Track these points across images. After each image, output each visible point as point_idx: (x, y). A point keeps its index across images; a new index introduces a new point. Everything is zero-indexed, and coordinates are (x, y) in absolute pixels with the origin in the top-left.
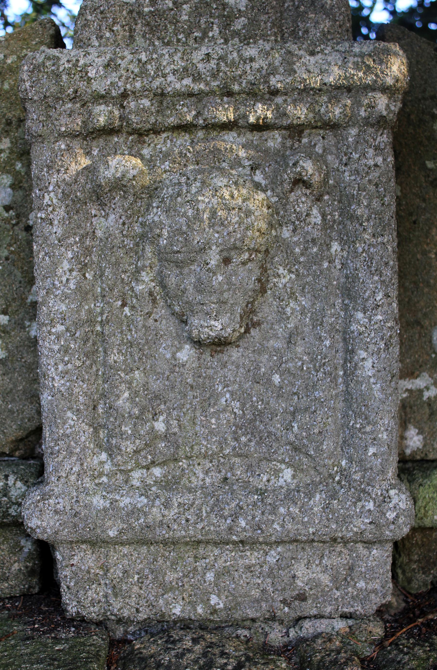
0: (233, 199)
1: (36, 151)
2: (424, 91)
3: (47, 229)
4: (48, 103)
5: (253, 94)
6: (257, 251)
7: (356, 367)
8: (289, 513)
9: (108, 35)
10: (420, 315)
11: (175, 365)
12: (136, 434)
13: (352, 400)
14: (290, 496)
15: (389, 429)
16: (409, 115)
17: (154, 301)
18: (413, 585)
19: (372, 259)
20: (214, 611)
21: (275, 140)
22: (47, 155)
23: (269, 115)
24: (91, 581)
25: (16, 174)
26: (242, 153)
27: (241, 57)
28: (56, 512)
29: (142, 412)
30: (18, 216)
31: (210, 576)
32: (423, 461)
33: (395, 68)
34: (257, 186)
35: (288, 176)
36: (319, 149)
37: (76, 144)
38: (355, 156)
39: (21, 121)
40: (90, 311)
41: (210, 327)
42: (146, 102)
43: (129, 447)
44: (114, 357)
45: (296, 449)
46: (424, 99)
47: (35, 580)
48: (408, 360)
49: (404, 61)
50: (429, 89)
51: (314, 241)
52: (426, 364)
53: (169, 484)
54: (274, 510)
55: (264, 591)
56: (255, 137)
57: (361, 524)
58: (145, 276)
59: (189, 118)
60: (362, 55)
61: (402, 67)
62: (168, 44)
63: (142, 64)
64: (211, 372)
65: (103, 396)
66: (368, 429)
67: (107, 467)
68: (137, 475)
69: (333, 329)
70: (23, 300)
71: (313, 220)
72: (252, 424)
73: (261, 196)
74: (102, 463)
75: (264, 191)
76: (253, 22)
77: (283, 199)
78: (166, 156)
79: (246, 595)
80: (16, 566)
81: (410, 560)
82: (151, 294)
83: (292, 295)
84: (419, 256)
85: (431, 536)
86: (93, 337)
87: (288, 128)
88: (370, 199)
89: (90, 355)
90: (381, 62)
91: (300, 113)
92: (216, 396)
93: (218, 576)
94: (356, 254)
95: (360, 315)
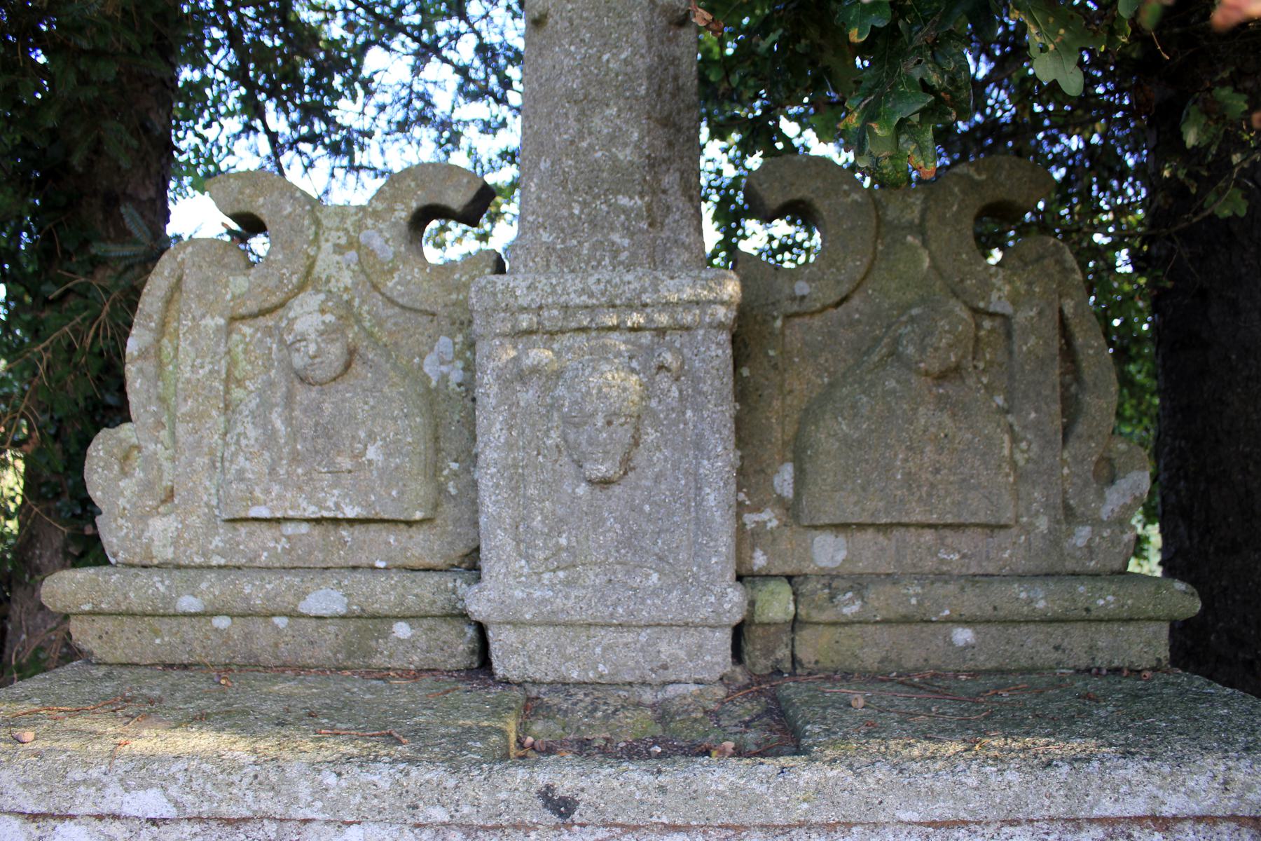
0: (617, 381)
1: (479, 345)
3: (485, 400)
4: (488, 313)
5: (630, 307)
6: (631, 416)
7: (703, 500)
8: (654, 604)
9: (531, 264)
11: (574, 498)
12: (546, 547)
13: (702, 524)
14: (655, 592)
17: (560, 451)
19: (714, 422)
20: (601, 676)
21: (646, 338)
22: (486, 350)
23: (642, 321)
24: (513, 652)
25: (466, 360)
26: (623, 347)
27: (621, 280)
28: (489, 600)
29: (550, 531)
30: (467, 391)
31: (598, 650)
32: (767, 576)
33: (730, 288)
34: (633, 371)
35: (654, 363)
36: (677, 345)
37: (507, 342)
38: (702, 349)
39: (470, 322)
40: (514, 459)
41: (598, 470)
42: (555, 312)
43: (541, 555)
44: (531, 491)
45: (660, 559)
47: (475, 658)
51: (673, 409)
53: (569, 583)
54: (643, 601)
55: (637, 662)
56: (632, 336)
57: (705, 612)
58: (553, 434)
59: (585, 323)
60: (707, 280)
62: (573, 271)
63: (553, 286)
64: (600, 503)
65: (523, 519)
66: (712, 544)
67: (525, 570)
68: (546, 576)
69: (687, 472)
70: (469, 452)
71: (672, 394)
72: (629, 541)
73: (634, 378)
74: (522, 567)
75: (638, 374)
76: (633, 255)
77: (652, 379)
78: (569, 349)
79: (625, 665)
80: (461, 647)
82: (557, 446)
83: (658, 448)
86: (516, 477)
87: (656, 329)
88: (713, 380)
89: (515, 489)
90: (720, 284)
91: (663, 319)
92: (604, 520)
93: (604, 650)
94: (703, 419)
95: (705, 462)
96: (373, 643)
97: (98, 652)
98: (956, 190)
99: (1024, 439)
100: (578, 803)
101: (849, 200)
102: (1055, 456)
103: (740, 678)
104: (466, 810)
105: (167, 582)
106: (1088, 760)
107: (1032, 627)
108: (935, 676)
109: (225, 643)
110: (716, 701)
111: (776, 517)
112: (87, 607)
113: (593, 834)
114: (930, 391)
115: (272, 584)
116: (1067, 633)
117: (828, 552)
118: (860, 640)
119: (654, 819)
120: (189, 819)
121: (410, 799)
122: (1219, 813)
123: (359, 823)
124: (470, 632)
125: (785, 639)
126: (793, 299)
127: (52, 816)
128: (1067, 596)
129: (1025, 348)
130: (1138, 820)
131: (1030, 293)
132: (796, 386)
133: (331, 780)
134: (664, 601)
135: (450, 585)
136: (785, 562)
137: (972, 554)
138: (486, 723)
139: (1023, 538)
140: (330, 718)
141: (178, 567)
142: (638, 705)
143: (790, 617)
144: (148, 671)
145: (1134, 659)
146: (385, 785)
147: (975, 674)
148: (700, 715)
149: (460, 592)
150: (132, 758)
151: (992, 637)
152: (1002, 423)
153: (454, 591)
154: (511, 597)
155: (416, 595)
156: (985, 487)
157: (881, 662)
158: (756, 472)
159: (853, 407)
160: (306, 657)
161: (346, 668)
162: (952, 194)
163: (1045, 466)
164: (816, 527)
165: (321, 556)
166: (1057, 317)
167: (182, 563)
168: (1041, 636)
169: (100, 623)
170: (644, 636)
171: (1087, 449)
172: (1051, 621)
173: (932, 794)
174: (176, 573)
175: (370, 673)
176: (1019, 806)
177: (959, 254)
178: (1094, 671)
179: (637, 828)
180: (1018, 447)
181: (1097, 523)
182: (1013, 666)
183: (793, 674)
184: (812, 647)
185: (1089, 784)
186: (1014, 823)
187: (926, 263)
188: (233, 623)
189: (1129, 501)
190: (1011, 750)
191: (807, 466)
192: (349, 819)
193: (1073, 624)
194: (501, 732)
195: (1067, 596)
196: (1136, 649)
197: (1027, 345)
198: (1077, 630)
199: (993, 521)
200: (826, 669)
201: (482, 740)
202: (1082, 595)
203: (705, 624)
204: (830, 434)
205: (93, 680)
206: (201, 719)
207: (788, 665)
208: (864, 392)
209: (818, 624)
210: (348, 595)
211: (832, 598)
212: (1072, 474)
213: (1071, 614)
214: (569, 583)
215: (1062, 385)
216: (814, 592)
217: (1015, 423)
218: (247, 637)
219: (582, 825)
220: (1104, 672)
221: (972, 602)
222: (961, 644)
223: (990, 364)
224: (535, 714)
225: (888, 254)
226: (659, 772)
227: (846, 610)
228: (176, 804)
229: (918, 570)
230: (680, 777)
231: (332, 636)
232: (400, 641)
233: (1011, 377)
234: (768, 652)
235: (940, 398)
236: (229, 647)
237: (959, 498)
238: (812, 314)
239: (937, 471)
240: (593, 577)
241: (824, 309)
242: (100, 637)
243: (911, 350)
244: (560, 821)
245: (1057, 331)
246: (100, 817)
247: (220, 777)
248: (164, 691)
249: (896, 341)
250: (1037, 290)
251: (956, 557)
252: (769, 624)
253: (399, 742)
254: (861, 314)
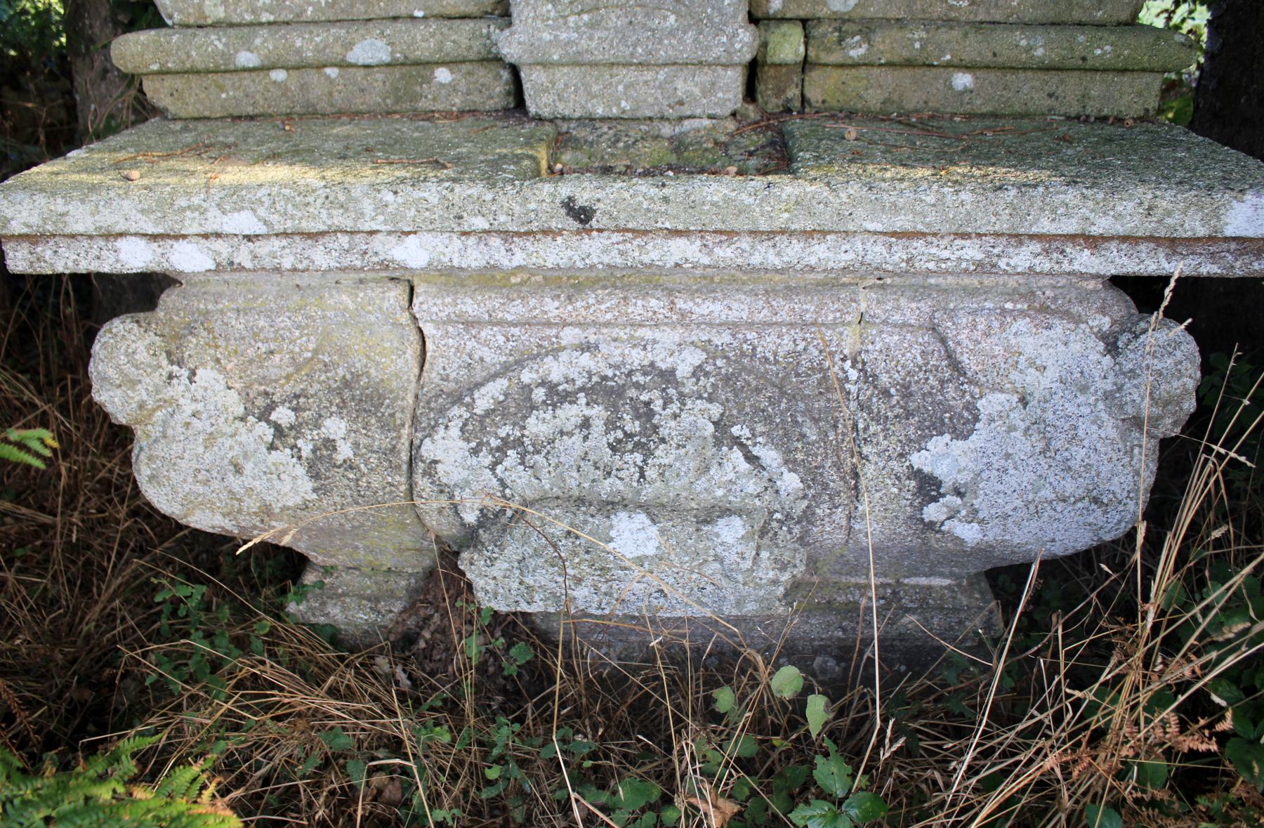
14: (672, 33)
20: (624, 112)
31: (621, 88)
47: (511, 99)
53: (593, 25)
54: (661, 41)
55: (656, 98)
57: (718, 52)
68: (572, 19)
74: (549, 11)
79: (645, 101)
80: (498, 89)
93: (626, 87)
96: (418, 88)
97: (172, 108)
100: (595, 211)
103: (752, 115)
104: (502, 218)
105: (224, 40)
106: (1035, 186)
107: (1030, 74)
108: (932, 117)
109: (284, 94)
110: (728, 134)
112: (155, 67)
113: (609, 238)
115: (320, 37)
116: (1062, 81)
118: (865, 82)
119: (659, 225)
120: (277, 235)
121: (456, 210)
122: (1139, 234)
123: (415, 233)
124: (506, 75)
127: (168, 236)
130: (1072, 238)
133: (389, 197)
134: (680, 41)
135: (485, 31)
138: (519, 151)
140: (384, 151)
141: (231, 25)
142: (657, 137)
143: (801, 58)
144: (219, 123)
145: (1123, 109)
146: (434, 199)
147: (970, 116)
148: (710, 145)
149: (494, 37)
150: (223, 187)
151: (991, 82)
153: (488, 36)
154: (540, 39)
155: (454, 42)
160: (359, 103)
161: (395, 112)
165: (362, 8)
167: (234, 21)
168: (1037, 84)
169: (169, 82)
170: (662, 75)
172: (1048, 69)
173: (895, 209)
174: (231, 31)
175: (417, 115)
176: (969, 222)
179: (645, 232)
183: (801, 112)
184: (820, 87)
185: (1032, 205)
186: (965, 236)
188: (289, 75)
190: (972, 176)
192: (406, 229)
194: (533, 158)
196: (1127, 98)
198: (1072, 79)
200: (832, 109)
201: (514, 163)
203: (717, 63)
205: (173, 132)
206: (274, 157)
207: (797, 104)
209: (826, 65)
210: (391, 44)
211: (840, 41)
213: (1068, 63)
214: (593, 25)
216: (824, 35)
218: (303, 87)
219: (600, 231)
220: (1092, 119)
221: (974, 47)
222: (960, 88)
224: (565, 146)
226: (664, 185)
227: (853, 53)
228: (265, 222)
229: (927, 16)
230: (681, 190)
231: (380, 84)
232: (442, 85)
234: (780, 91)
236: (288, 98)
240: (615, 20)
242: (172, 95)
244: (580, 226)
246: (206, 236)
247: (298, 199)
248: (237, 137)
252: (780, 65)
253: (445, 167)
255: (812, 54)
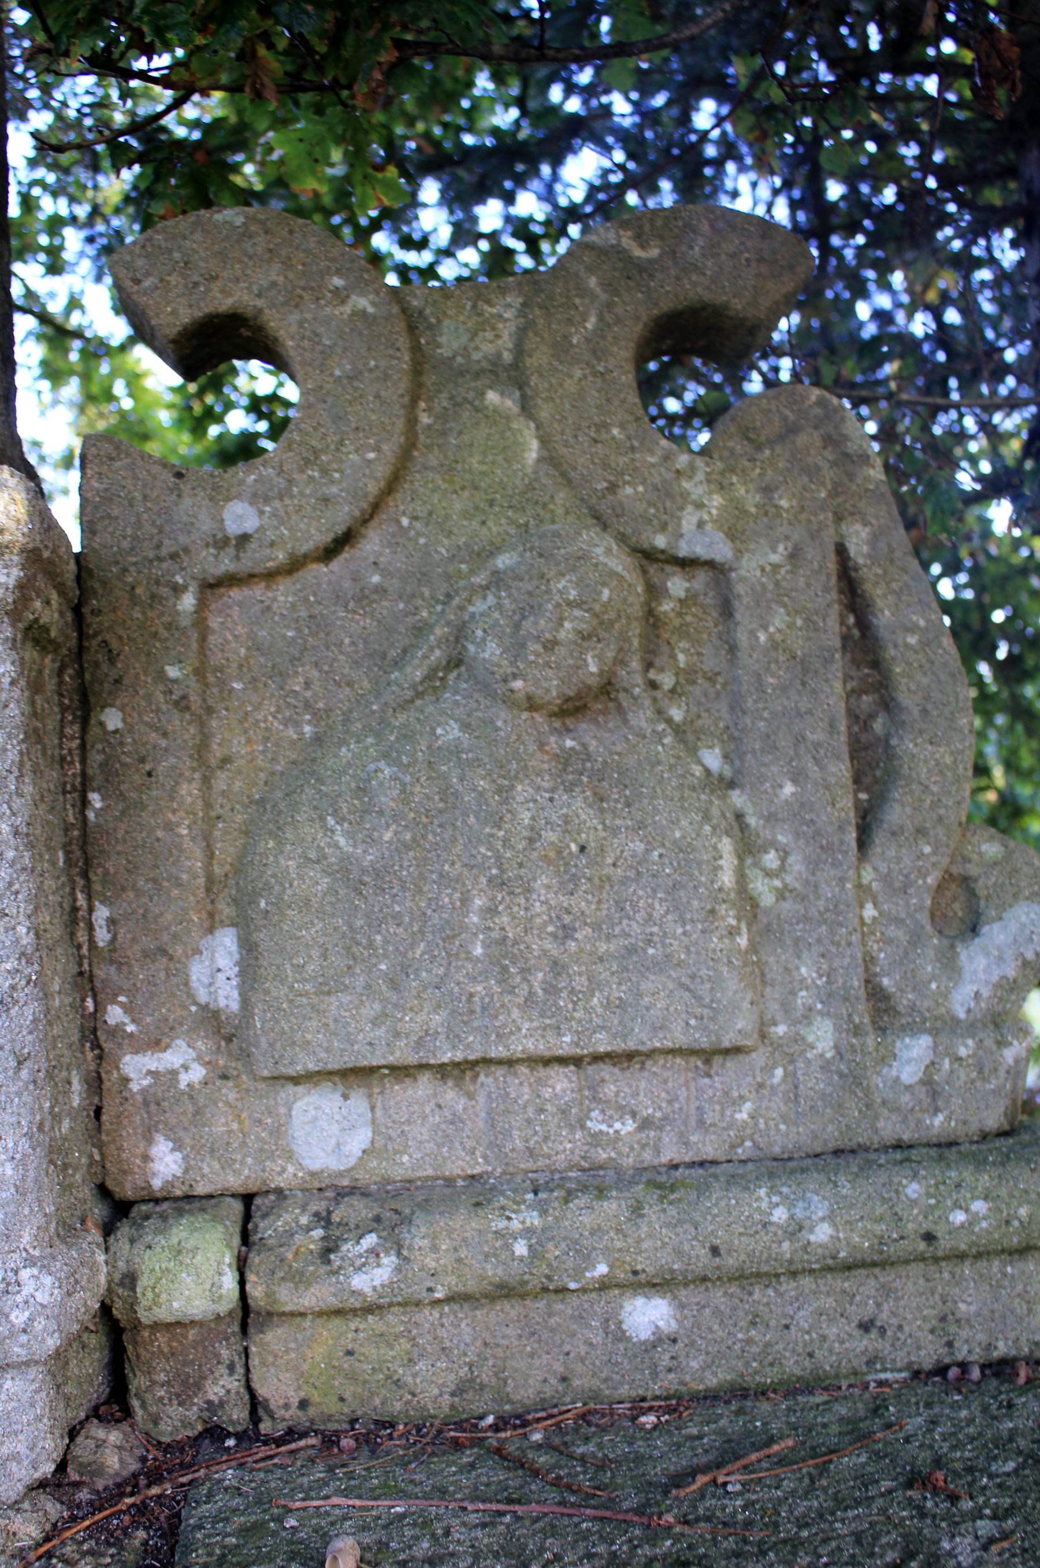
2: (158, 547)
10: (166, 937)
15: (18, 1156)
16: (133, 588)
18: (162, 1427)
32: (188, 1198)
46: (160, 559)
48: (148, 1019)
49: (18, 497)
50: (166, 542)
52: (181, 1024)
61: (12, 508)
81: (153, 1382)
84: (160, 834)
85: (186, 1337)
98: (593, 282)
99: (773, 844)
101: (347, 309)
102: (842, 880)
111: (199, 1059)
114: (542, 745)
116: (887, 1291)
117: (327, 1135)
118: (405, 1344)
125: (225, 1353)
126: (221, 543)
128: (880, 1210)
129: (762, 637)
131: (768, 510)
132: (238, 746)
136: (227, 1164)
137: (665, 1118)
139: (779, 1072)
147: (676, 1404)
151: (717, 1312)
152: (715, 811)
156: (680, 964)
157: (459, 1391)
158: (146, 954)
159: (362, 791)
162: (583, 291)
163: (821, 904)
164: (296, 1080)
166: (832, 564)
168: (830, 1302)
171: (912, 857)
177: (605, 426)
178: (953, 1373)
180: (756, 864)
181: (943, 1027)
182: (770, 1377)
184: (289, 1374)
187: (533, 451)
189: (1011, 971)
191: (261, 937)
193: (902, 1270)
195: (880, 1210)
197: (765, 629)
198: (910, 1283)
199: (704, 1042)
202: (914, 1203)
204: (310, 857)
208: (386, 756)
211: (328, 1249)
212: (886, 918)
213: (891, 1250)
215: (852, 716)
217: (749, 809)
220: (976, 1374)
221: (661, 1236)
223: (689, 675)
225: (444, 433)
229: (541, 1163)
233: (736, 706)
234: (187, 1387)
235: (565, 760)
237: (618, 992)
238: (270, 576)
239: (567, 932)
241: (295, 565)
243: (492, 651)
245: (834, 595)
249: (460, 633)
250: (784, 503)
251: (628, 1126)
254: (385, 573)
255: (256, 1291)
